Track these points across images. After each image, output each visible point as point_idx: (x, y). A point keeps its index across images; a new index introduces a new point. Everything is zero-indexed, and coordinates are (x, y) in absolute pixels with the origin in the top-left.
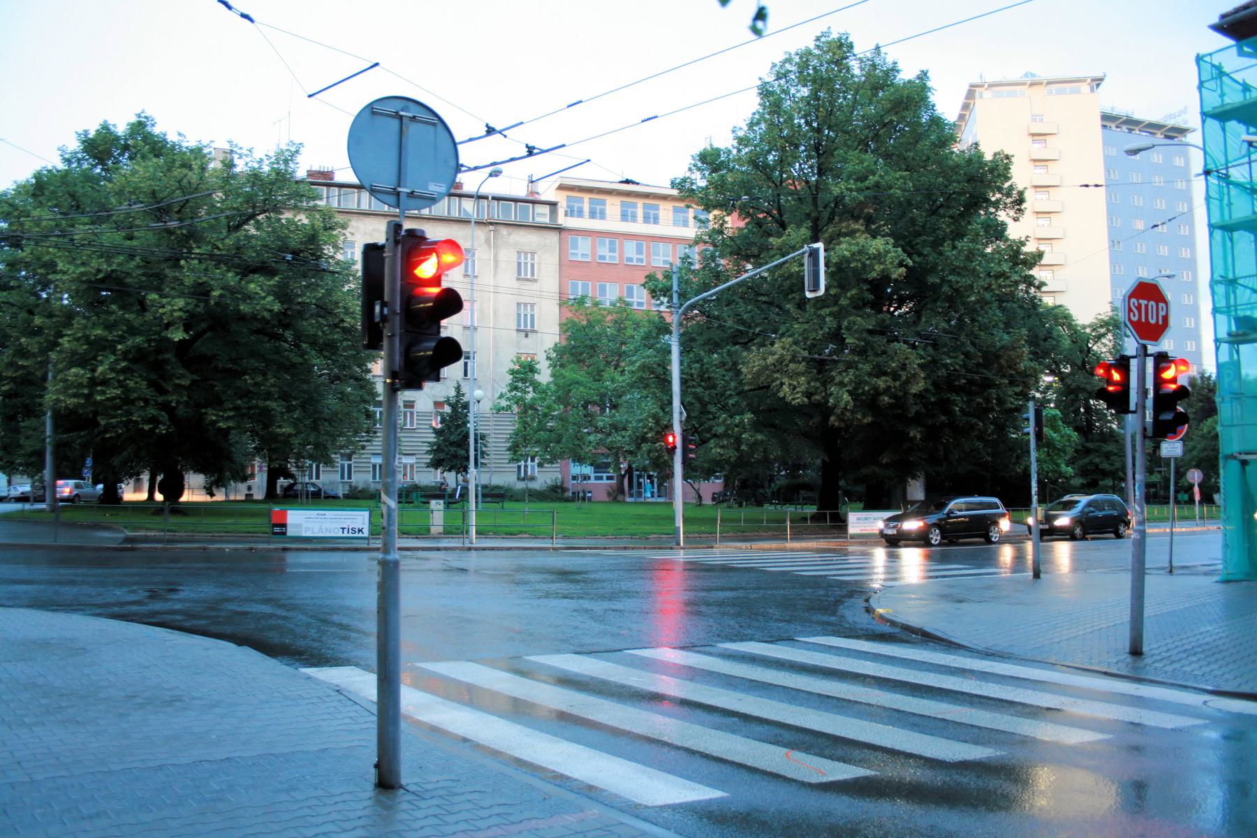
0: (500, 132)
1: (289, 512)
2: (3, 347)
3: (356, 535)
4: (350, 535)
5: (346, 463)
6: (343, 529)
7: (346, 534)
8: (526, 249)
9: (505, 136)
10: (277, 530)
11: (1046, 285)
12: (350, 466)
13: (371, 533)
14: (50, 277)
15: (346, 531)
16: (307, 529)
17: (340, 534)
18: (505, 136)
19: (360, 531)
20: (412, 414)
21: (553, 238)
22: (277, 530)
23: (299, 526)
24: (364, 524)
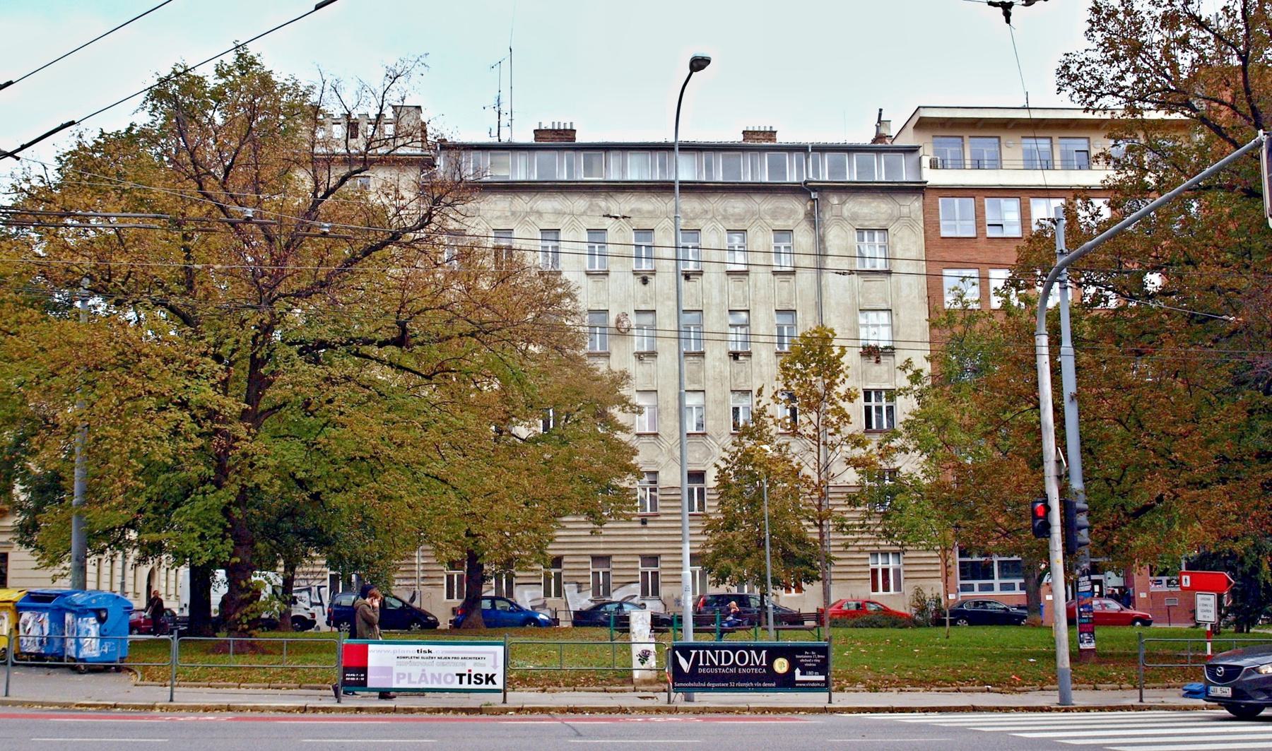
0: (12, 154)
1: (371, 647)
2: (7, 333)
3: (483, 686)
4: (473, 686)
5: (650, 570)
6: (461, 676)
7: (465, 685)
8: (867, 224)
9: (18, 159)
10: (351, 677)
11: (921, 371)
12: (606, 574)
13: (508, 682)
14: (1140, 39)
15: (465, 679)
16: (401, 676)
17: (456, 685)
18: (18, 159)
19: (490, 679)
20: (701, 492)
21: (913, 205)
22: (351, 677)
23: (387, 671)
24: (495, 667)
